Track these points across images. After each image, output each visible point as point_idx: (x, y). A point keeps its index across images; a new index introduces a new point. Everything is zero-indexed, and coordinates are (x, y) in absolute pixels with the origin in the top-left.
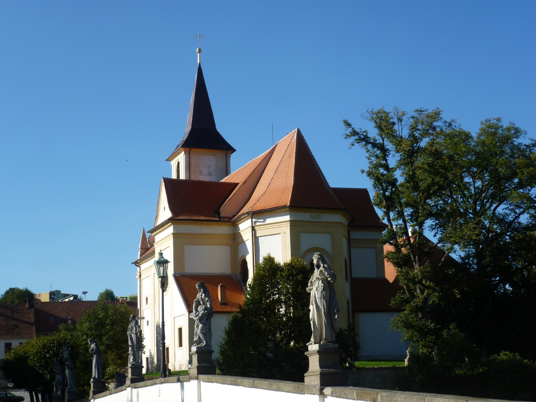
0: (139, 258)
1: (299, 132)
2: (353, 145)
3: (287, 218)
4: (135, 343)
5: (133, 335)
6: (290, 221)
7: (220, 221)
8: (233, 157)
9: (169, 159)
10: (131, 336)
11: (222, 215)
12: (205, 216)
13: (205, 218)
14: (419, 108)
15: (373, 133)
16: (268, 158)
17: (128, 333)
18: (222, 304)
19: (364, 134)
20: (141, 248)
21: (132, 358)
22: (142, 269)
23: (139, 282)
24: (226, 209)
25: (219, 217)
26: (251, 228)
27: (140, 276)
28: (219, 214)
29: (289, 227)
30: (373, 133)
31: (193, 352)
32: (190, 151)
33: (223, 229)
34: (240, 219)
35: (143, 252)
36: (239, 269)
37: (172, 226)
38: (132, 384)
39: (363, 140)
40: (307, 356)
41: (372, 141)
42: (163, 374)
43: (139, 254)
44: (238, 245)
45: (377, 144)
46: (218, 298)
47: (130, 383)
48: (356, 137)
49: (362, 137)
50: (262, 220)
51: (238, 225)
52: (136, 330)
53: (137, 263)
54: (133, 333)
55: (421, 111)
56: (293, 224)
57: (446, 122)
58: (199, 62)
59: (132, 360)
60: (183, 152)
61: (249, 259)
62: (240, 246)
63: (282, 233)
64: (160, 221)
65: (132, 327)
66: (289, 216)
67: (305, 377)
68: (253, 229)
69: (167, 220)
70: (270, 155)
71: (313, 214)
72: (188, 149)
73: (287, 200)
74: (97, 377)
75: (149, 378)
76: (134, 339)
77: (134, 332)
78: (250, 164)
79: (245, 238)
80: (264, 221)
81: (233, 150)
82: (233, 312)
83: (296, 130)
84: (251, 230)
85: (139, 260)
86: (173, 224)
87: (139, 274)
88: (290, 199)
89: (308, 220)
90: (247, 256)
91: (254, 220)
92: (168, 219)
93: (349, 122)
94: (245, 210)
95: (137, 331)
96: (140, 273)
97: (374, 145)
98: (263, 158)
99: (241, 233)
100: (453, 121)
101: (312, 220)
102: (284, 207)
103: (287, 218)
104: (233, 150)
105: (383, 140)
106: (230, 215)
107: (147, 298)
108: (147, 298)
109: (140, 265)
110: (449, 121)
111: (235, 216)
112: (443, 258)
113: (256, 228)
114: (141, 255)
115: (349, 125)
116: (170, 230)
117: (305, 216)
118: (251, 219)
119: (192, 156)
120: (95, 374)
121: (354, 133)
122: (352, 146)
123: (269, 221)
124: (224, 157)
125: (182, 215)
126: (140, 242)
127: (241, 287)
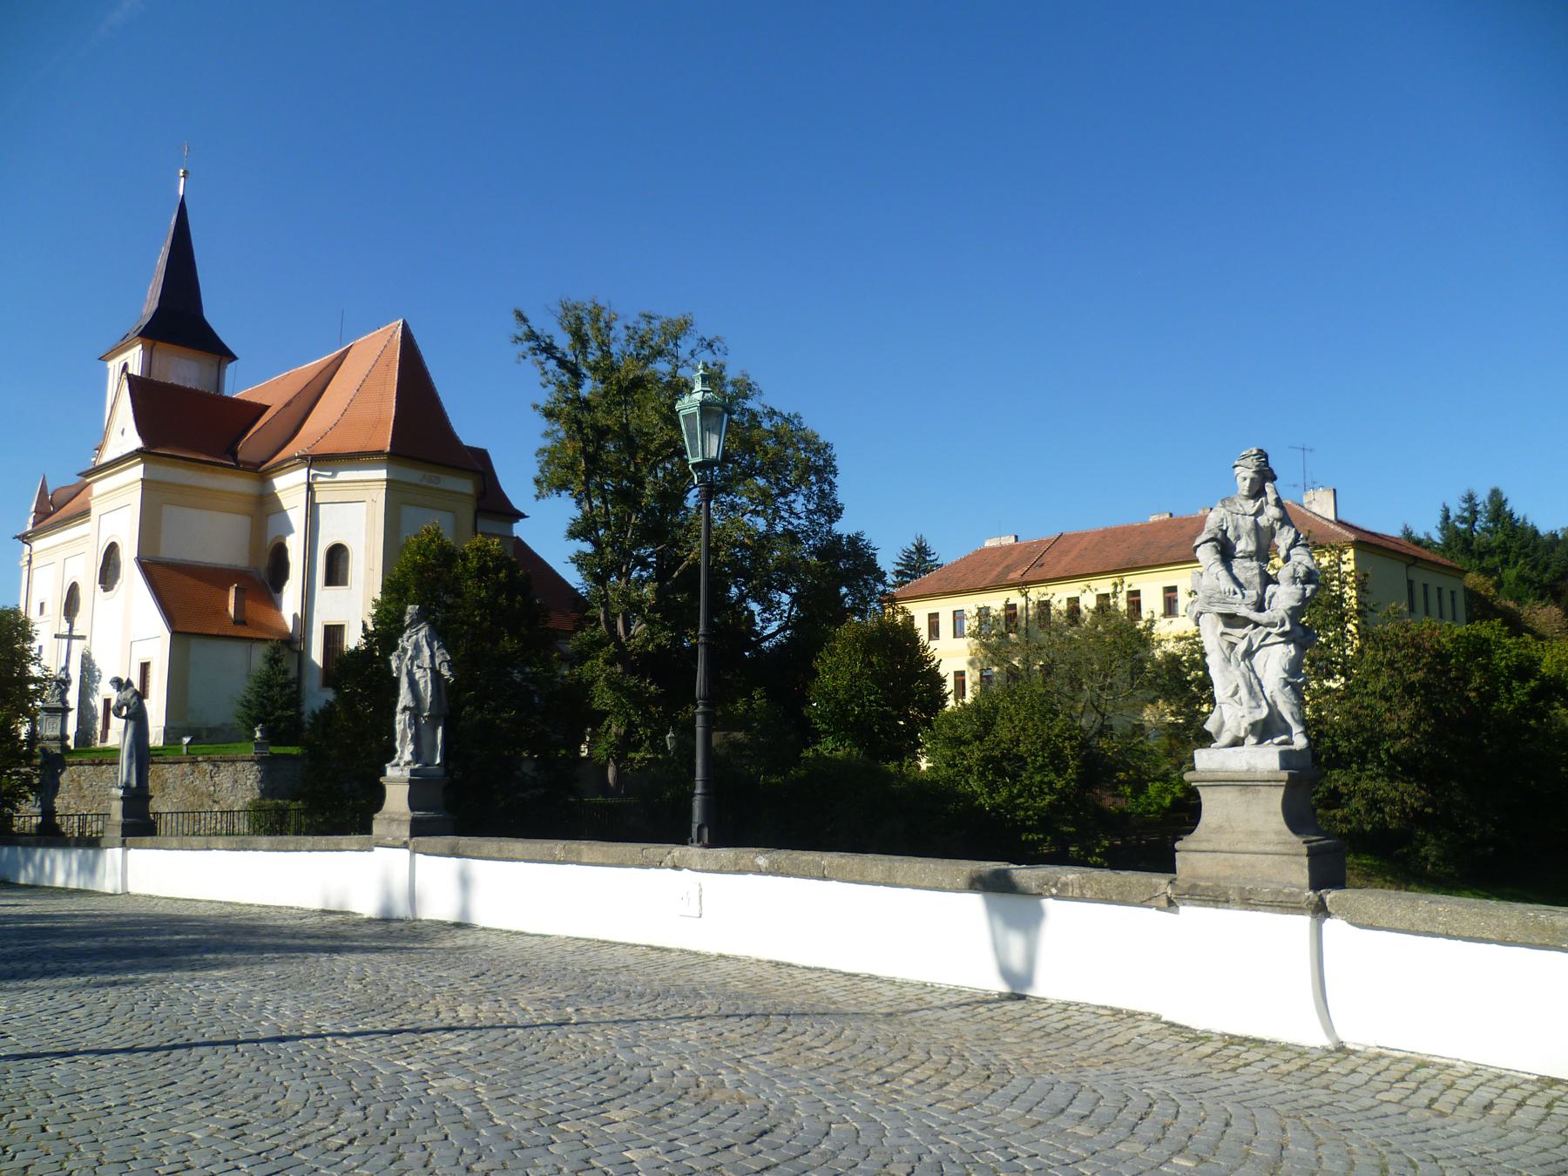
0: (29, 528)
1: (405, 325)
2: (524, 358)
3: (382, 474)
4: (429, 700)
5: (418, 674)
6: (387, 480)
7: (236, 467)
8: (230, 369)
9: (105, 358)
10: (410, 674)
11: (240, 457)
12: (207, 454)
13: (210, 459)
14: (646, 312)
15: (563, 342)
16: (332, 367)
17: (394, 665)
18: (236, 622)
19: (548, 341)
20: (35, 511)
21: (410, 748)
22: (34, 551)
23: (25, 574)
24: (249, 447)
25: (235, 459)
26: (305, 486)
27: (30, 562)
28: (234, 455)
29: (384, 491)
30: (563, 342)
31: (1203, 776)
32: (152, 348)
33: (240, 484)
34: (282, 467)
35: (37, 520)
36: (265, 561)
37: (142, 466)
38: (415, 839)
39: (544, 350)
40: (1193, 784)
41: (558, 355)
42: (706, 831)
43: (31, 520)
44: (268, 516)
45: (568, 362)
46: (227, 610)
47: (408, 833)
48: (532, 344)
49: (543, 344)
50: (330, 474)
51: (271, 479)
52: (432, 657)
53: (25, 538)
54: (419, 667)
55: (650, 317)
56: (391, 485)
57: (703, 339)
58: (181, 194)
59: (407, 757)
60: (140, 347)
61: (295, 546)
62: (273, 521)
63: (368, 500)
64: (109, 455)
65: (417, 647)
66: (385, 471)
67: (1177, 854)
68: (310, 487)
69: (132, 452)
70: (338, 362)
71: (427, 474)
72: (150, 342)
73: (384, 440)
74: (134, 783)
75: (93, 761)
76: (422, 686)
77: (427, 663)
78: (283, 378)
79: (286, 503)
80: (334, 475)
81: (232, 357)
82: (271, 640)
83: (401, 321)
84: (305, 490)
85: (30, 532)
86: (143, 461)
87: (28, 558)
88: (389, 441)
89: (418, 482)
90: (288, 538)
91: (312, 472)
92: (137, 450)
93: (525, 314)
94: (294, 448)
95: (437, 661)
96: (31, 556)
97: (562, 363)
98: (324, 366)
99: (279, 495)
100: (718, 338)
101: (424, 483)
102: (380, 453)
103: (382, 474)
104: (232, 357)
105: (576, 357)
106: (257, 460)
107: (42, 605)
108: (42, 605)
109: (32, 541)
110: (709, 337)
111: (267, 462)
112: (676, 573)
113: (315, 486)
114: (34, 524)
115: (521, 317)
116: (137, 472)
117: (413, 475)
118: (306, 469)
119: (156, 356)
120: (129, 774)
121: (532, 336)
122: (521, 359)
123: (343, 475)
124: (216, 368)
125: (163, 446)
126: (33, 499)
127: (270, 595)
